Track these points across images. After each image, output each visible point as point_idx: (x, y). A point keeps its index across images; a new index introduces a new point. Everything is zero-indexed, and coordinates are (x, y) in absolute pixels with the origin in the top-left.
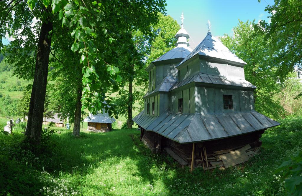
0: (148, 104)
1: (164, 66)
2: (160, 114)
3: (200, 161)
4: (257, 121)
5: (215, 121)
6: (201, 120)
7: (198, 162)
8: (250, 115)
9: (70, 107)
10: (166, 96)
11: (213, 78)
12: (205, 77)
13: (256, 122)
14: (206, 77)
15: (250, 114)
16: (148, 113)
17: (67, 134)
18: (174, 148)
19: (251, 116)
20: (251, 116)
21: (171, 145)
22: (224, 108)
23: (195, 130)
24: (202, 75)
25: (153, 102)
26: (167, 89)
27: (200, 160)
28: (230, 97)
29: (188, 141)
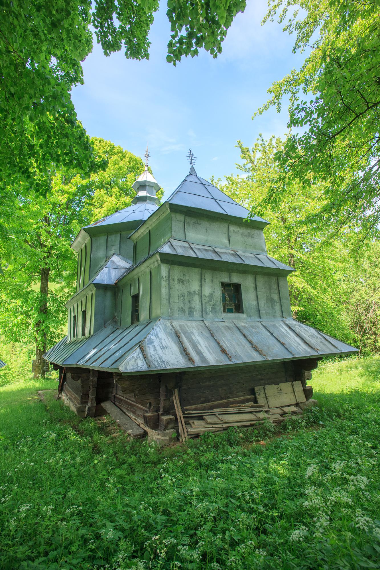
0: (75, 317)
1: (264, 389)
2: (94, 332)
3: (171, 419)
4: (298, 339)
5: (204, 332)
6: (171, 329)
7: (166, 420)
8: (281, 325)
9: (29, 194)
10: (109, 295)
11: (199, 249)
12: (180, 247)
13: (296, 341)
14: (184, 247)
15: (282, 323)
16: (74, 336)
17: (148, 25)
18: (121, 400)
19: (283, 328)
20: (283, 328)
21: (117, 396)
22: (224, 311)
23: (158, 347)
24: (174, 243)
25: (84, 309)
26: (110, 277)
27: (172, 417)
28: (237, 287)
29: (139, 369)
